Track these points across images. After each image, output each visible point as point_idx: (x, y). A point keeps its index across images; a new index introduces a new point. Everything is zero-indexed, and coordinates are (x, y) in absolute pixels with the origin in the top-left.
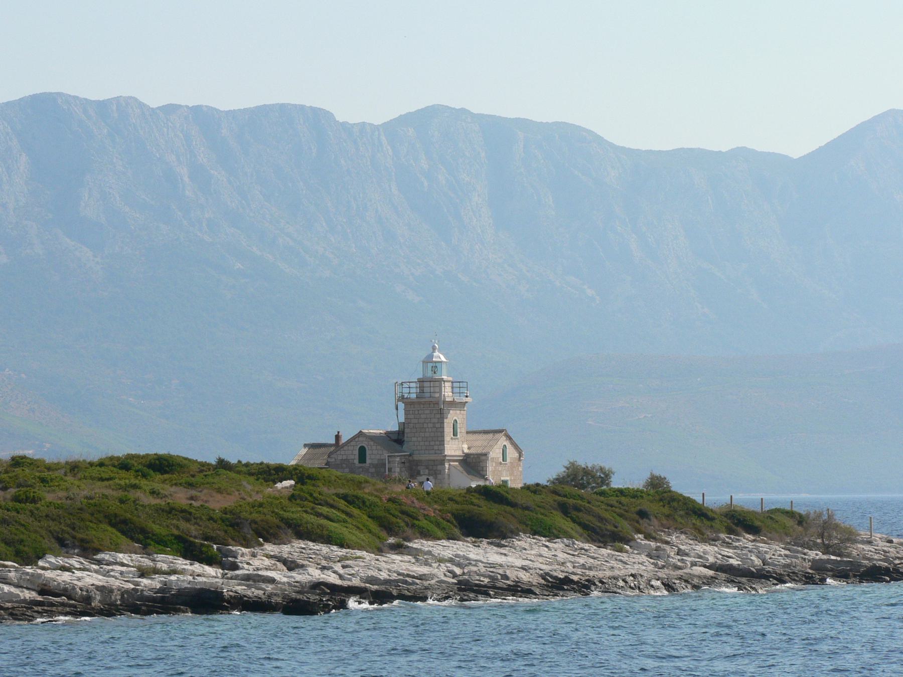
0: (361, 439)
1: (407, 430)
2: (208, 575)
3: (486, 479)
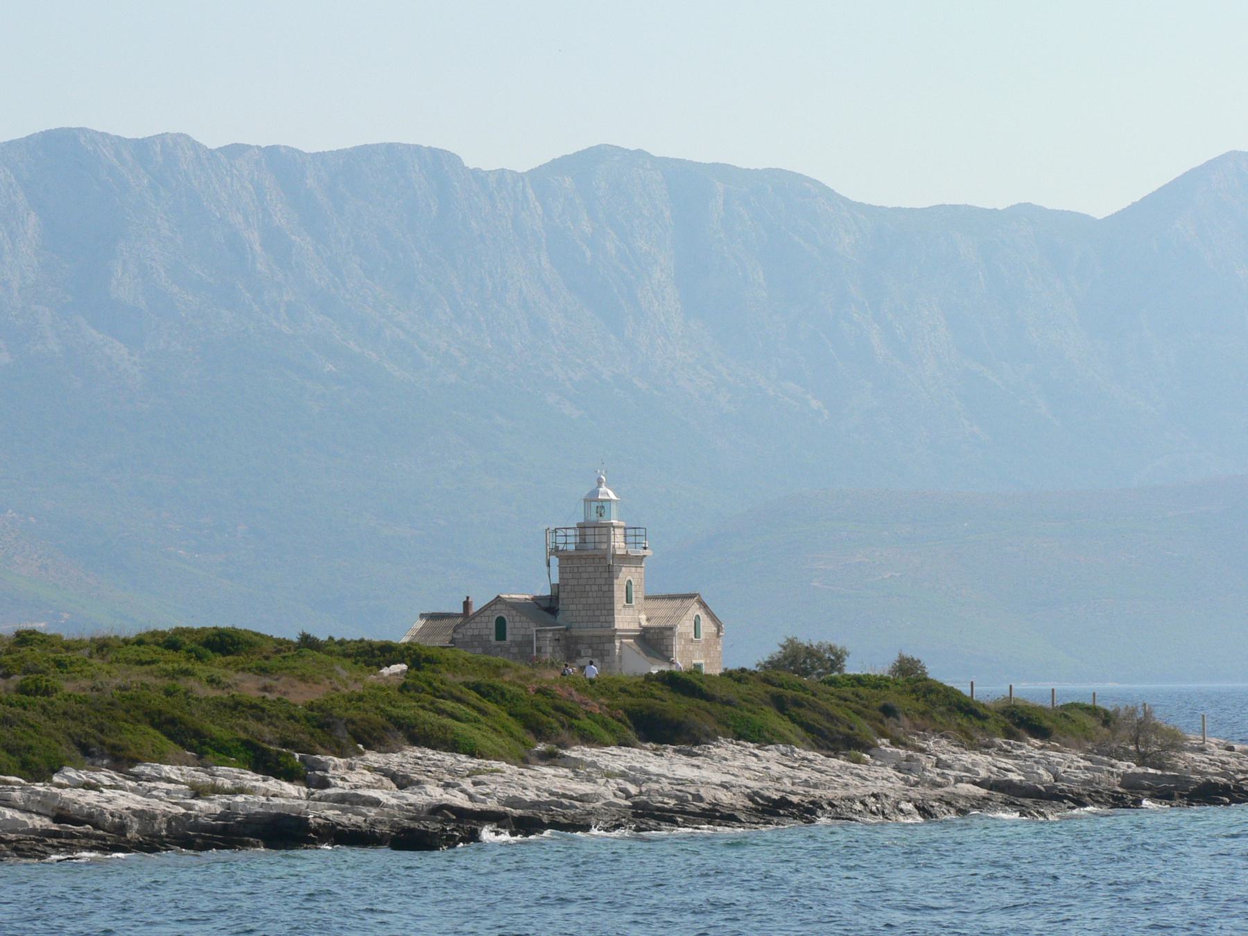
0: (498, 607)
1: (562, 595)
2: (288, 795)
3: (672, 663)
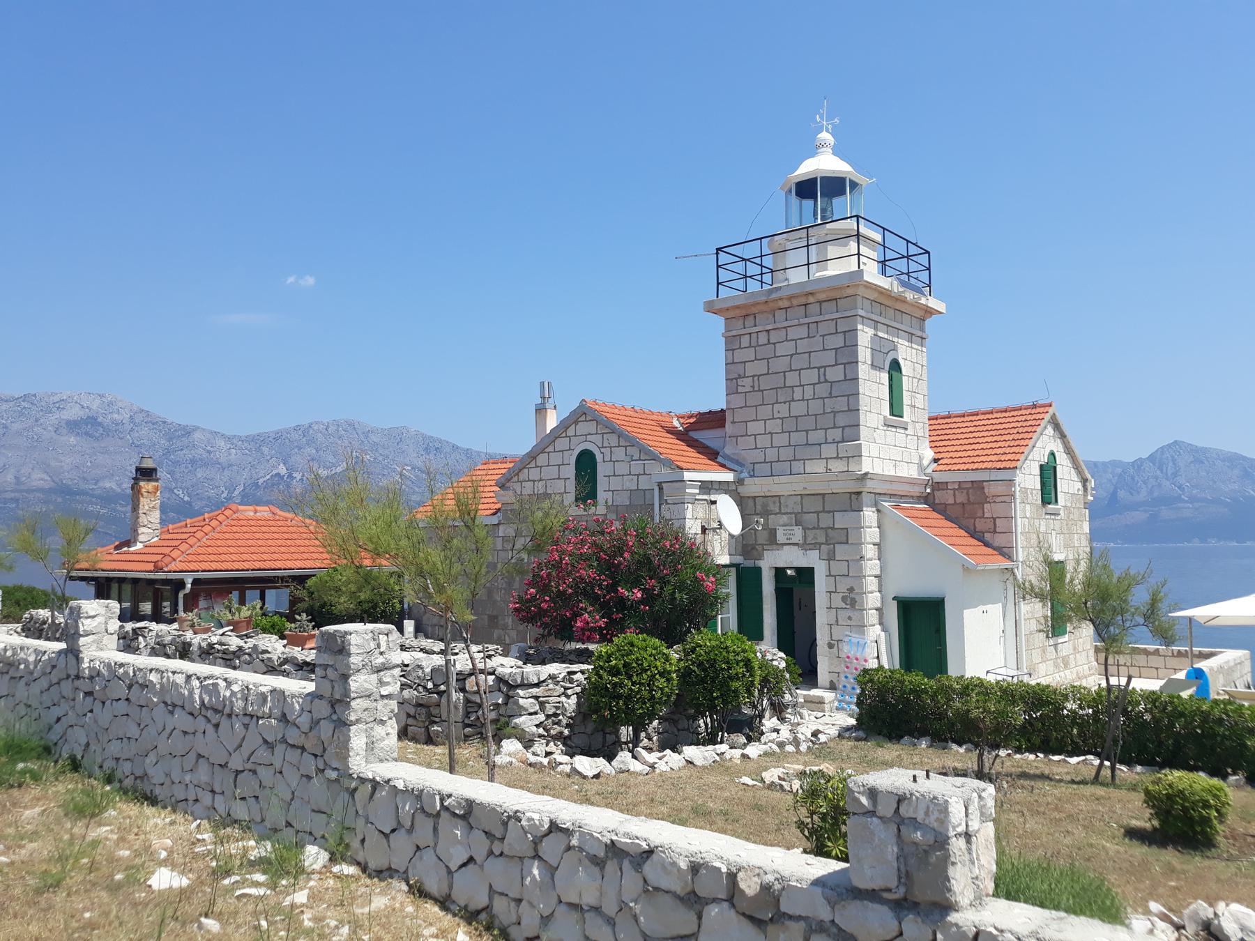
0: (583, 428)
3: (1052, 454)
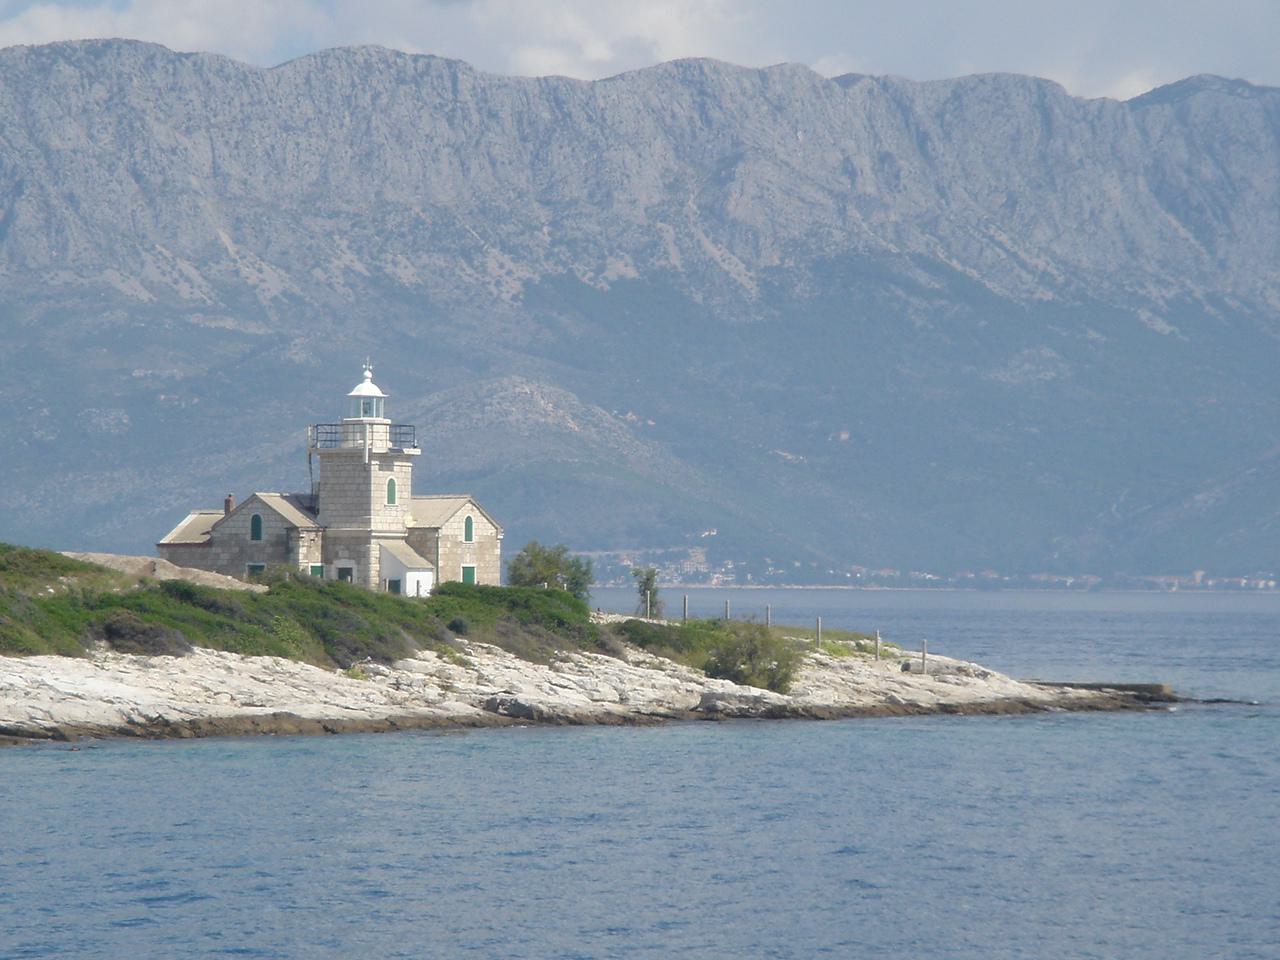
1: (322, 494)
2: (774, 698)
